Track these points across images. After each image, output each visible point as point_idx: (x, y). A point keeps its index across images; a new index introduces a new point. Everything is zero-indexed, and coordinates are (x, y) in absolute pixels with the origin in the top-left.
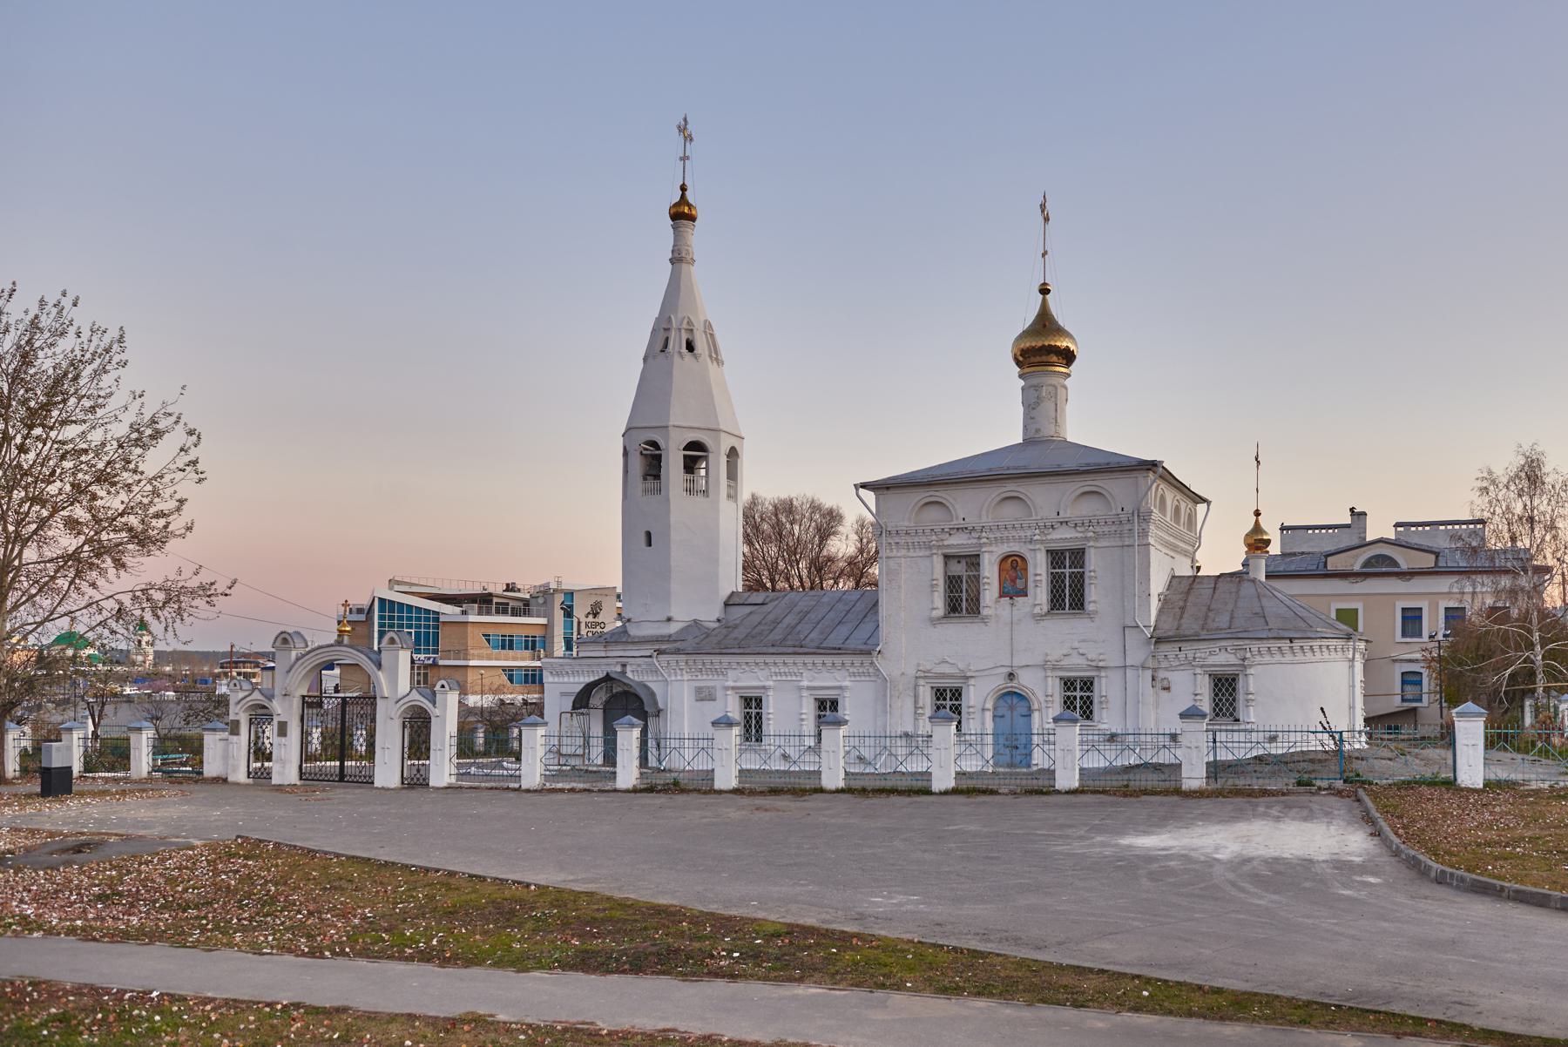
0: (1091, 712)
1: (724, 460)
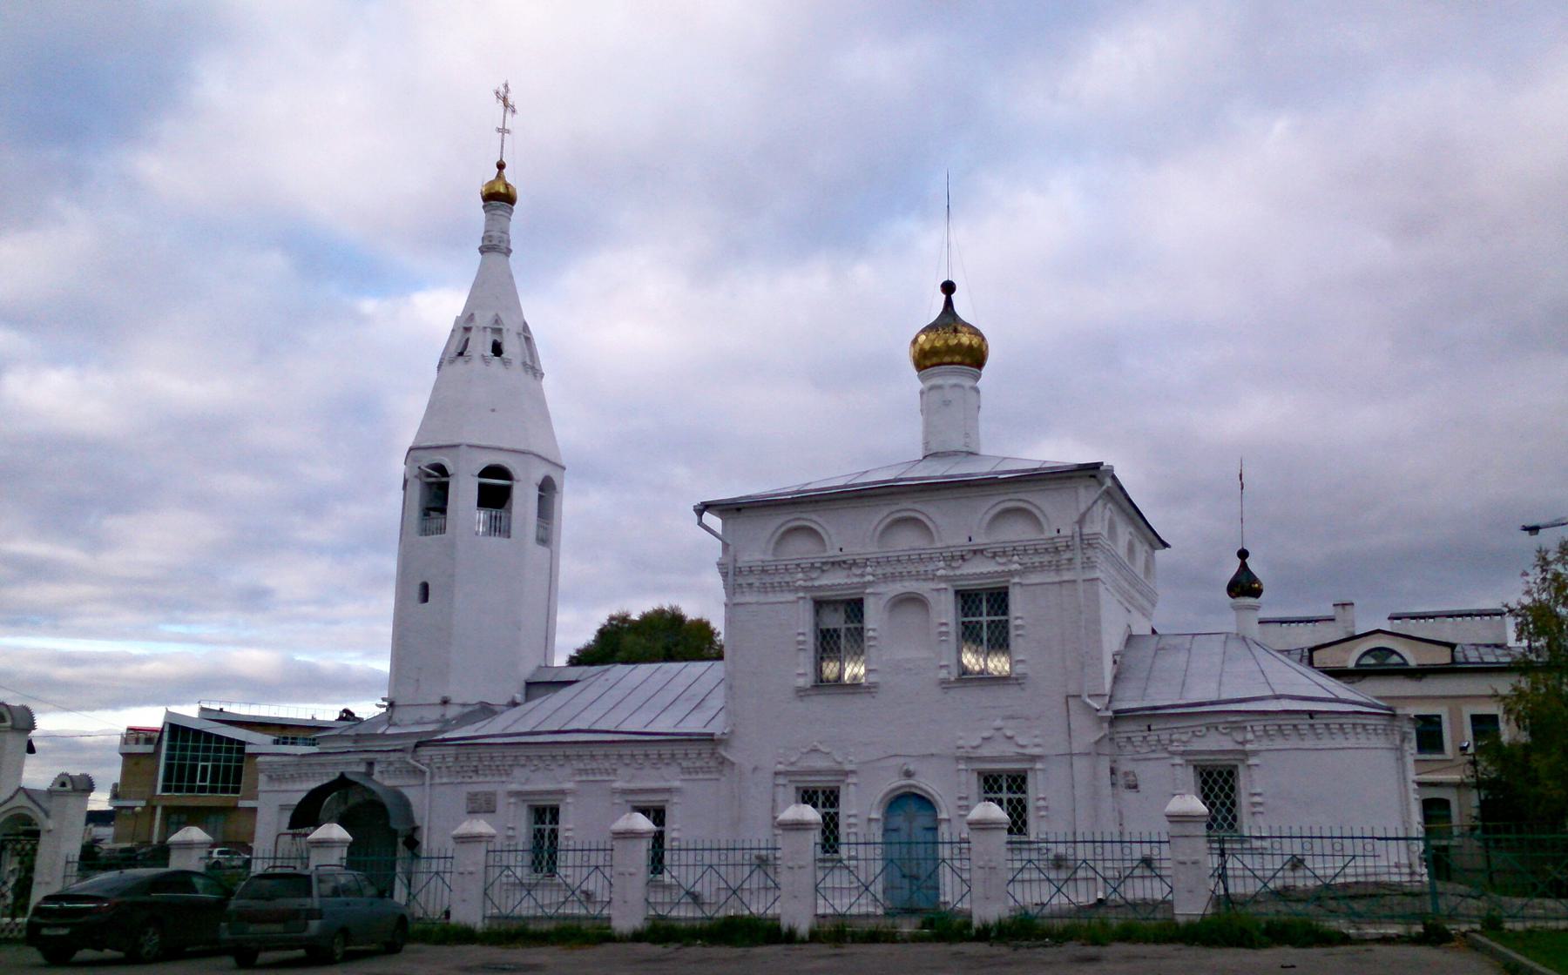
0: (1025, 823)
1: (535, 493)
